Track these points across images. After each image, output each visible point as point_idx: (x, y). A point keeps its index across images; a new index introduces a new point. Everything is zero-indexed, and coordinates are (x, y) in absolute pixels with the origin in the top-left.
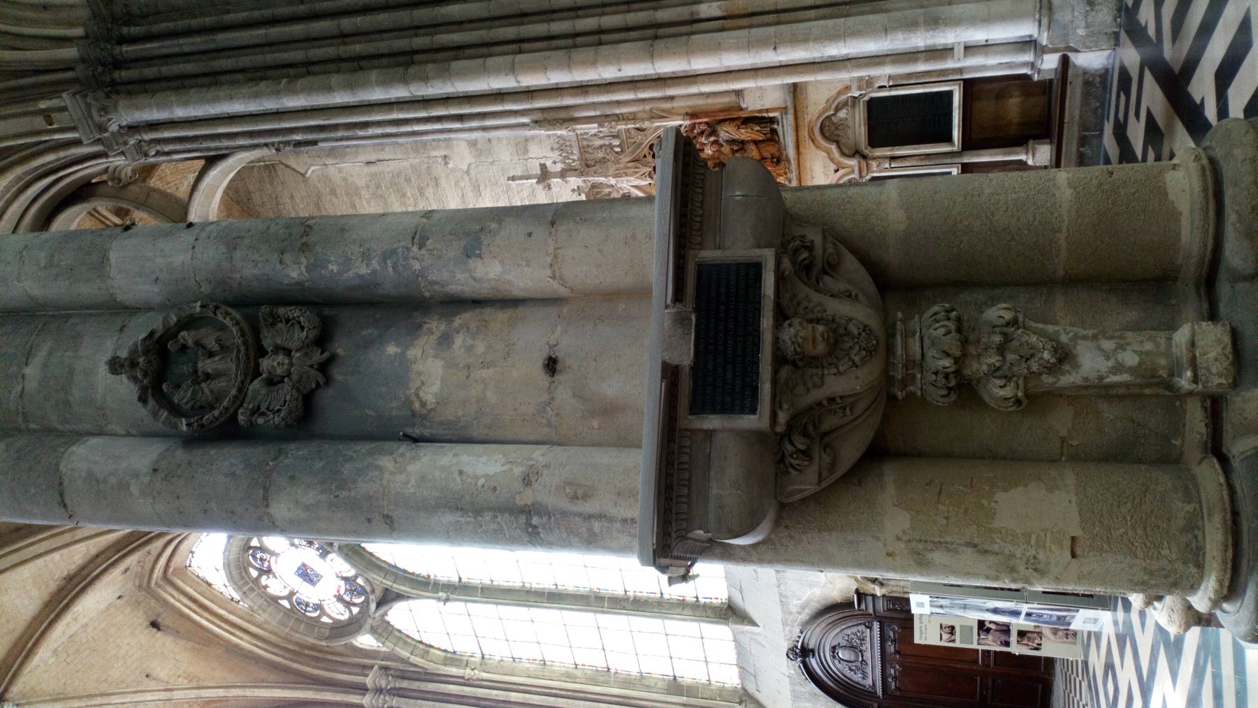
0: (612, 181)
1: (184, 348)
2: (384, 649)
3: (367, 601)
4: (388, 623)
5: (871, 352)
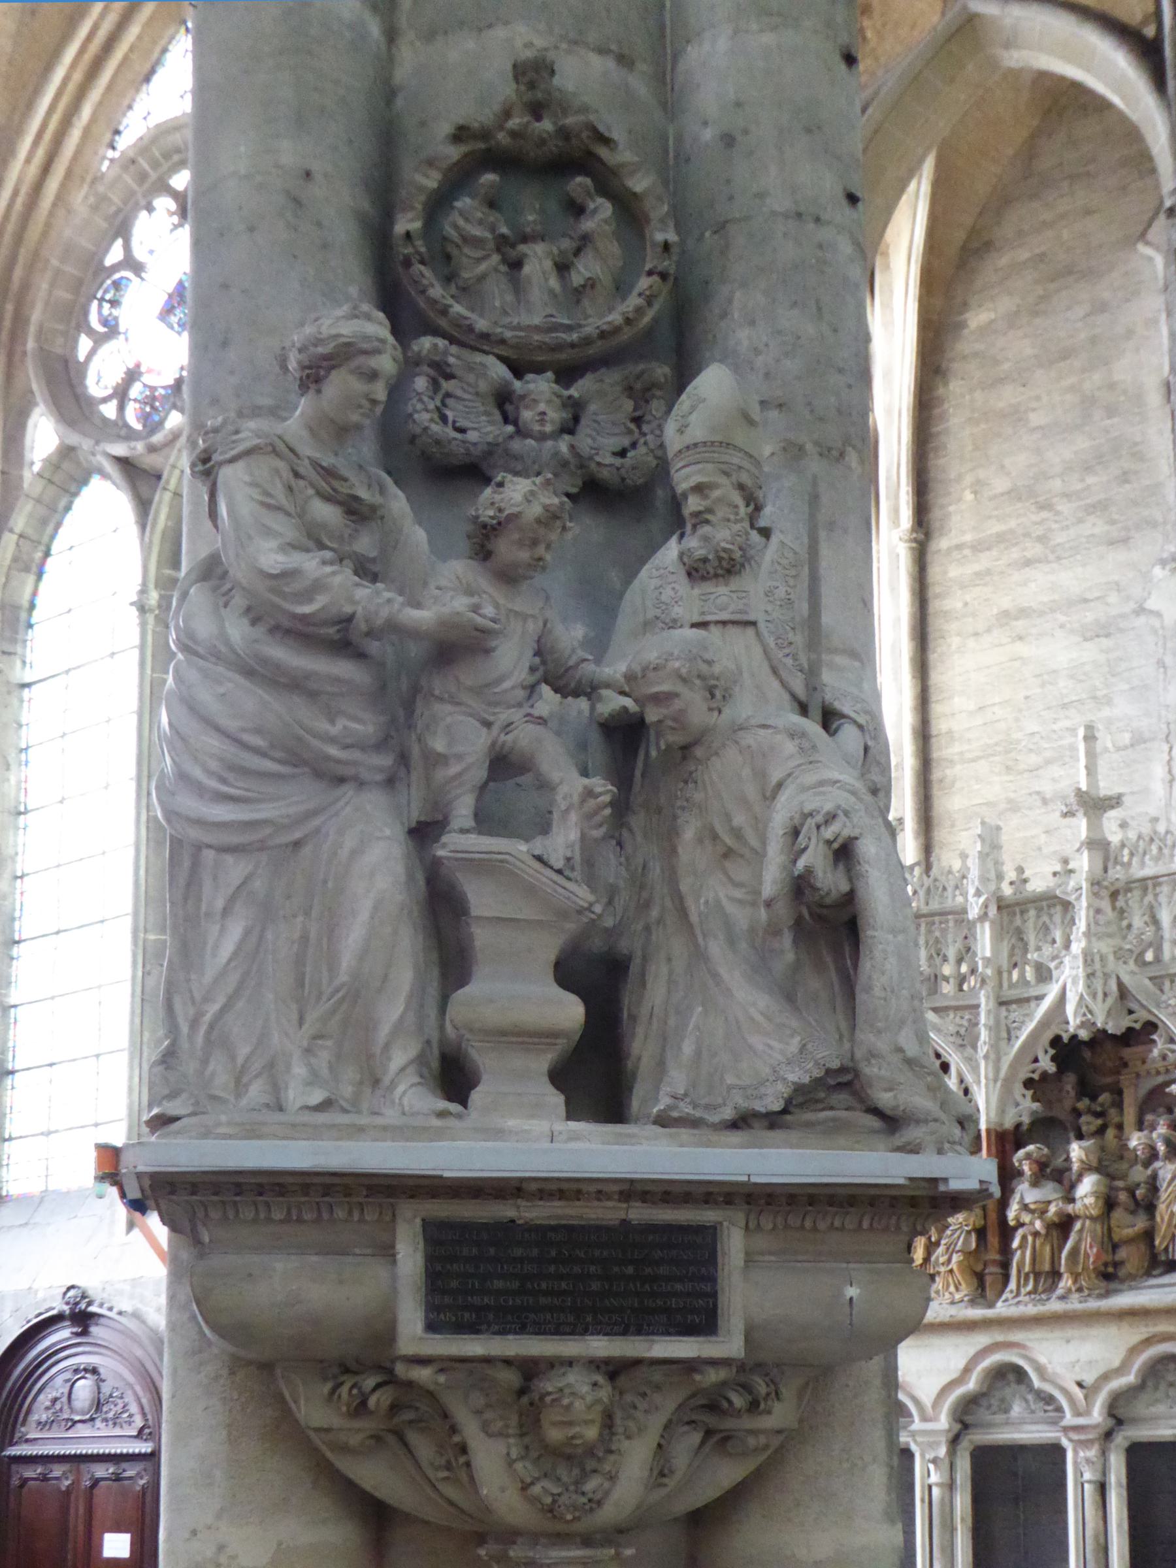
0: (1077, 947)
1: (577, 210)
2: (27, 476)
3: (130, 435)
4: (85, 481)
5: (550, 1511)
